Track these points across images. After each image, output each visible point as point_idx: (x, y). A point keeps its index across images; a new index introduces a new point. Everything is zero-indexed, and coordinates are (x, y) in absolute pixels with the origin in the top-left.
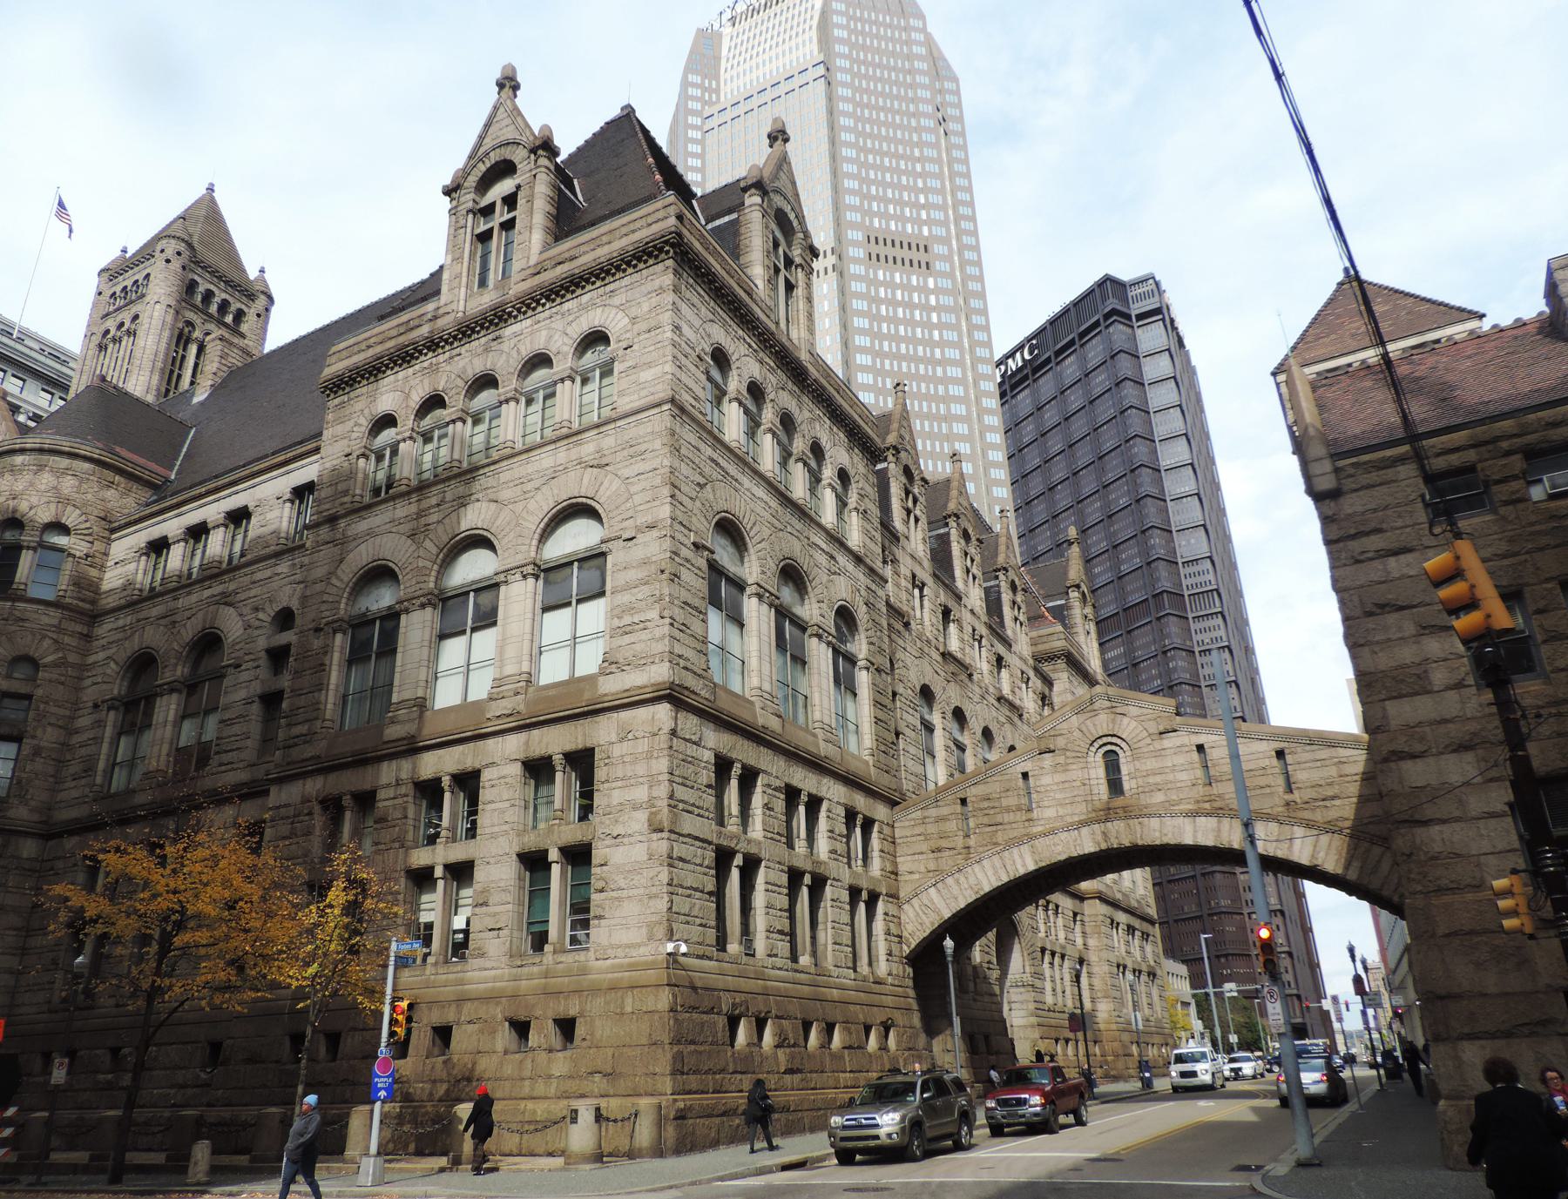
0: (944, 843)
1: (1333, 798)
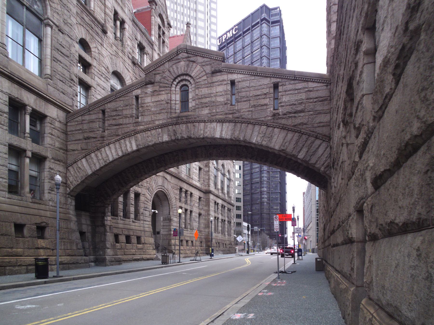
0: (92, 135)
1: (301, 111)
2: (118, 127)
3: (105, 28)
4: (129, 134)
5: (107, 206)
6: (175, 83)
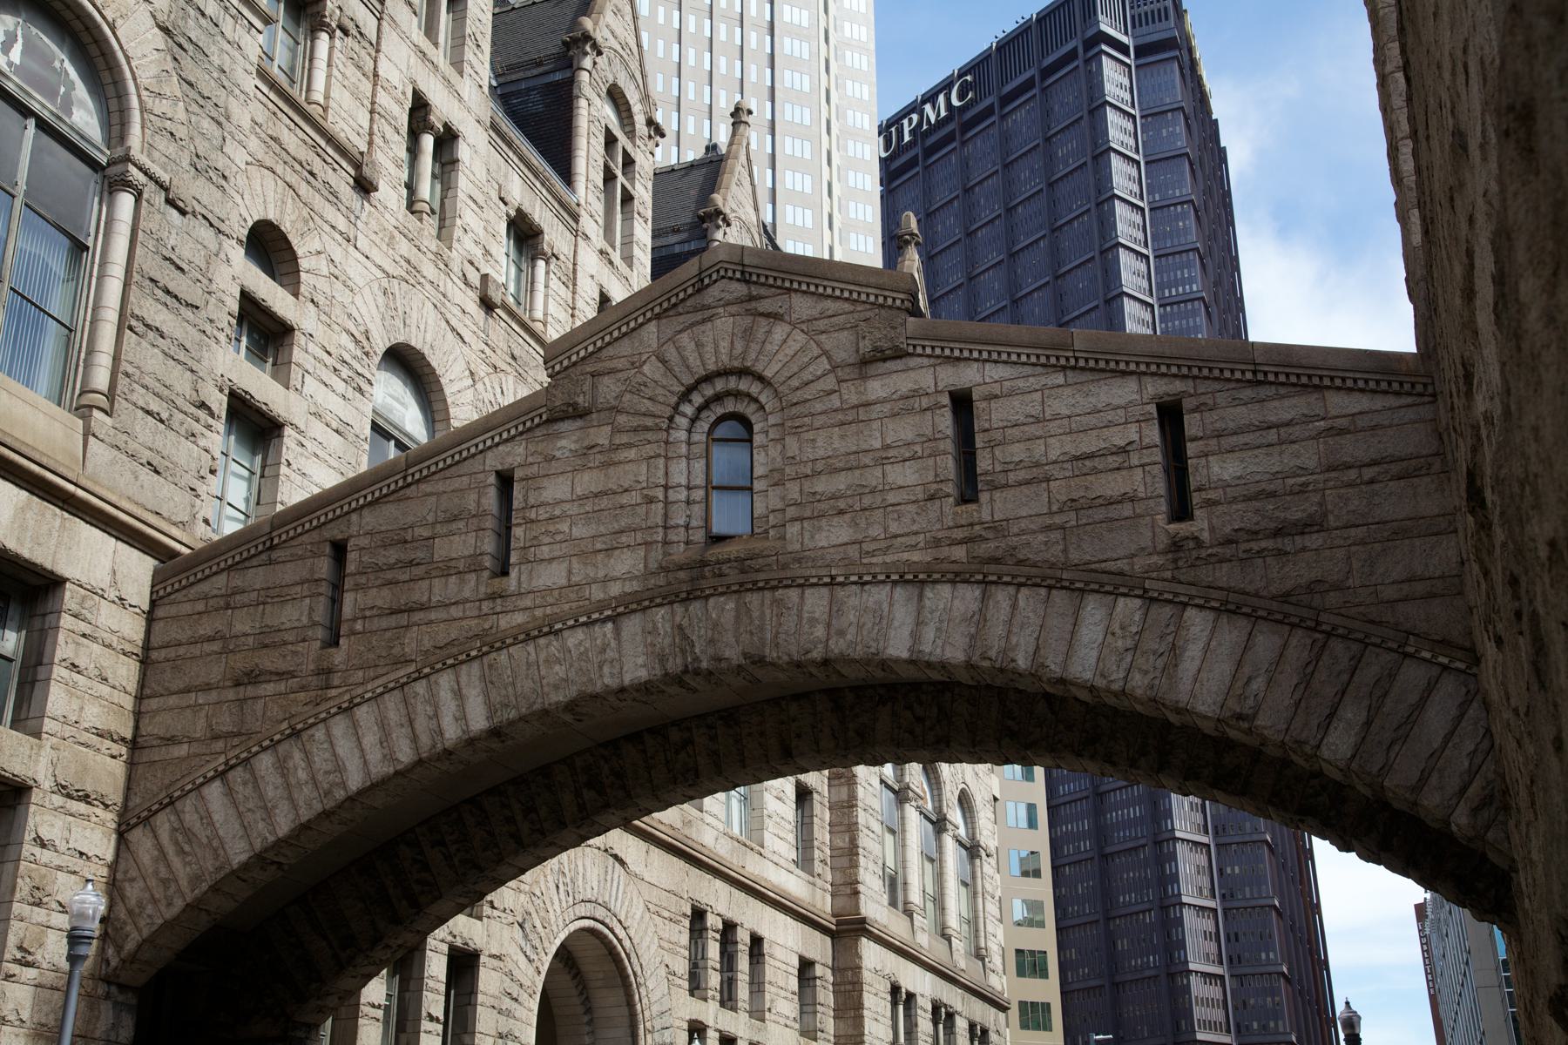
2: (403, 619)
3: (366, 171)
4: (455, 650)
5: (301, 1034)
6: (688, 409)
